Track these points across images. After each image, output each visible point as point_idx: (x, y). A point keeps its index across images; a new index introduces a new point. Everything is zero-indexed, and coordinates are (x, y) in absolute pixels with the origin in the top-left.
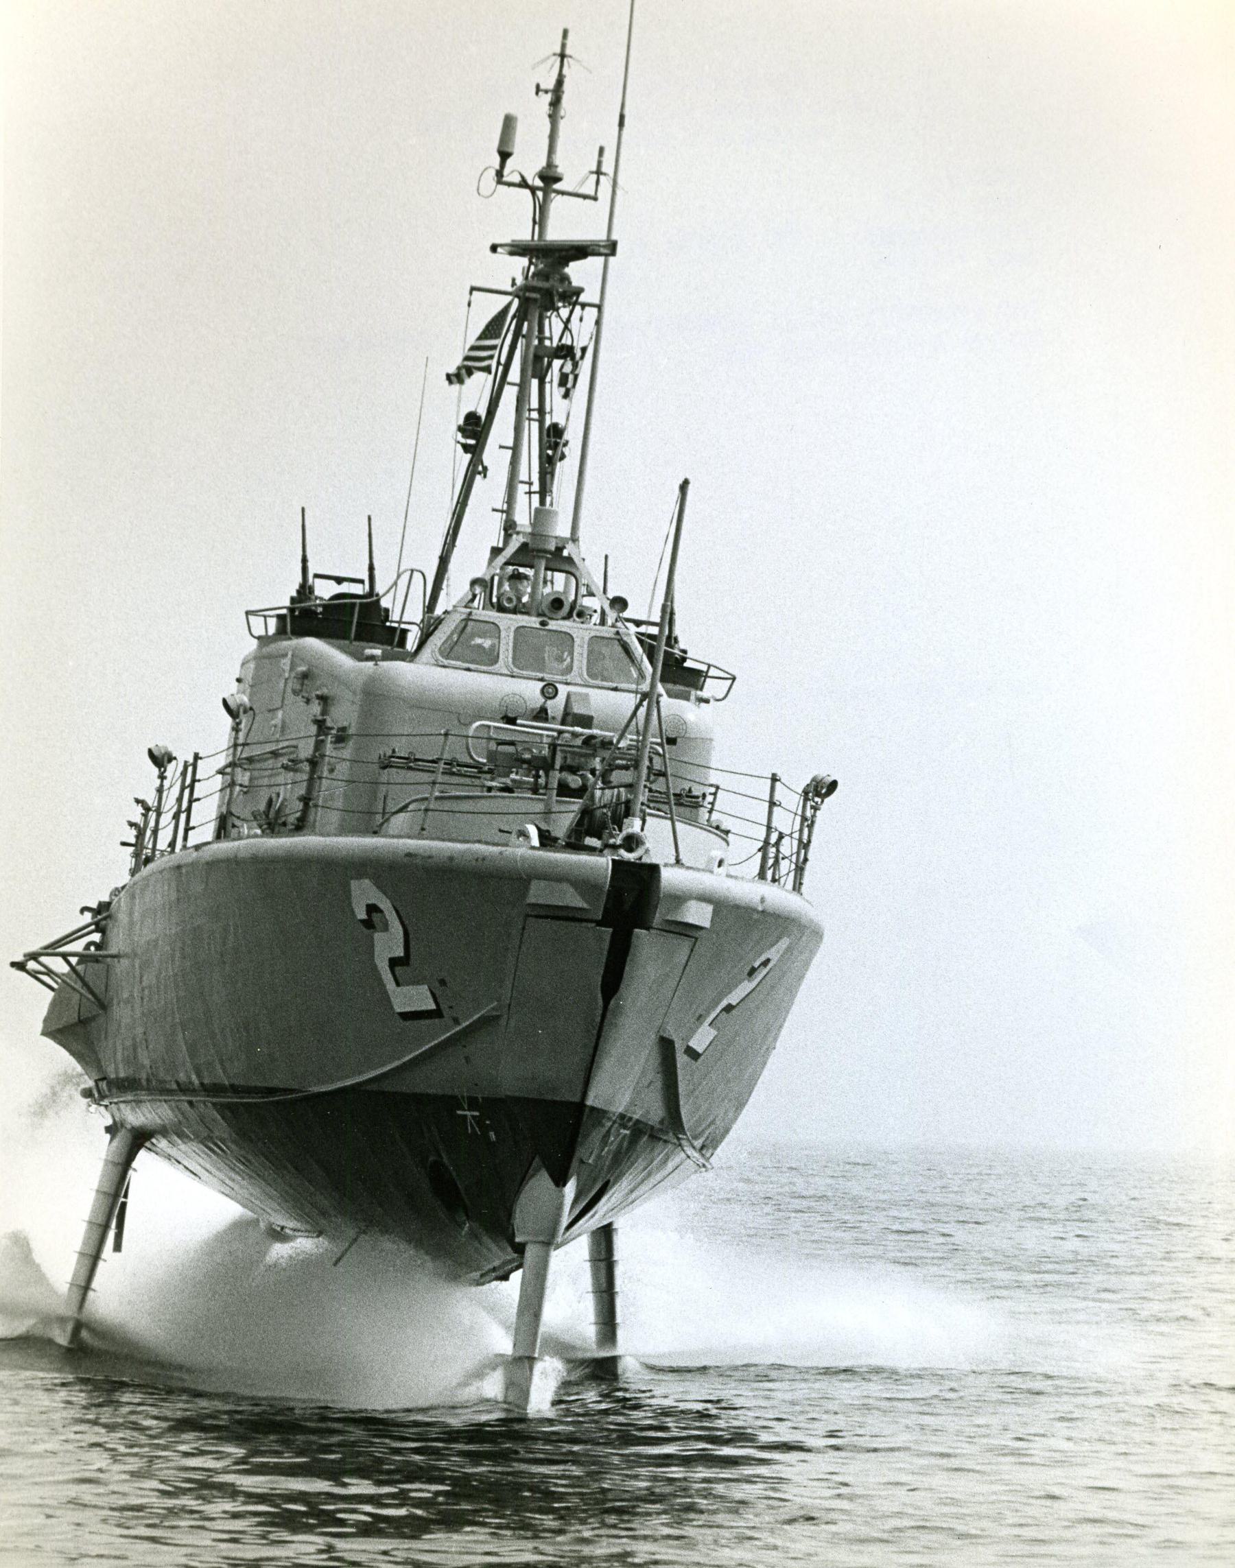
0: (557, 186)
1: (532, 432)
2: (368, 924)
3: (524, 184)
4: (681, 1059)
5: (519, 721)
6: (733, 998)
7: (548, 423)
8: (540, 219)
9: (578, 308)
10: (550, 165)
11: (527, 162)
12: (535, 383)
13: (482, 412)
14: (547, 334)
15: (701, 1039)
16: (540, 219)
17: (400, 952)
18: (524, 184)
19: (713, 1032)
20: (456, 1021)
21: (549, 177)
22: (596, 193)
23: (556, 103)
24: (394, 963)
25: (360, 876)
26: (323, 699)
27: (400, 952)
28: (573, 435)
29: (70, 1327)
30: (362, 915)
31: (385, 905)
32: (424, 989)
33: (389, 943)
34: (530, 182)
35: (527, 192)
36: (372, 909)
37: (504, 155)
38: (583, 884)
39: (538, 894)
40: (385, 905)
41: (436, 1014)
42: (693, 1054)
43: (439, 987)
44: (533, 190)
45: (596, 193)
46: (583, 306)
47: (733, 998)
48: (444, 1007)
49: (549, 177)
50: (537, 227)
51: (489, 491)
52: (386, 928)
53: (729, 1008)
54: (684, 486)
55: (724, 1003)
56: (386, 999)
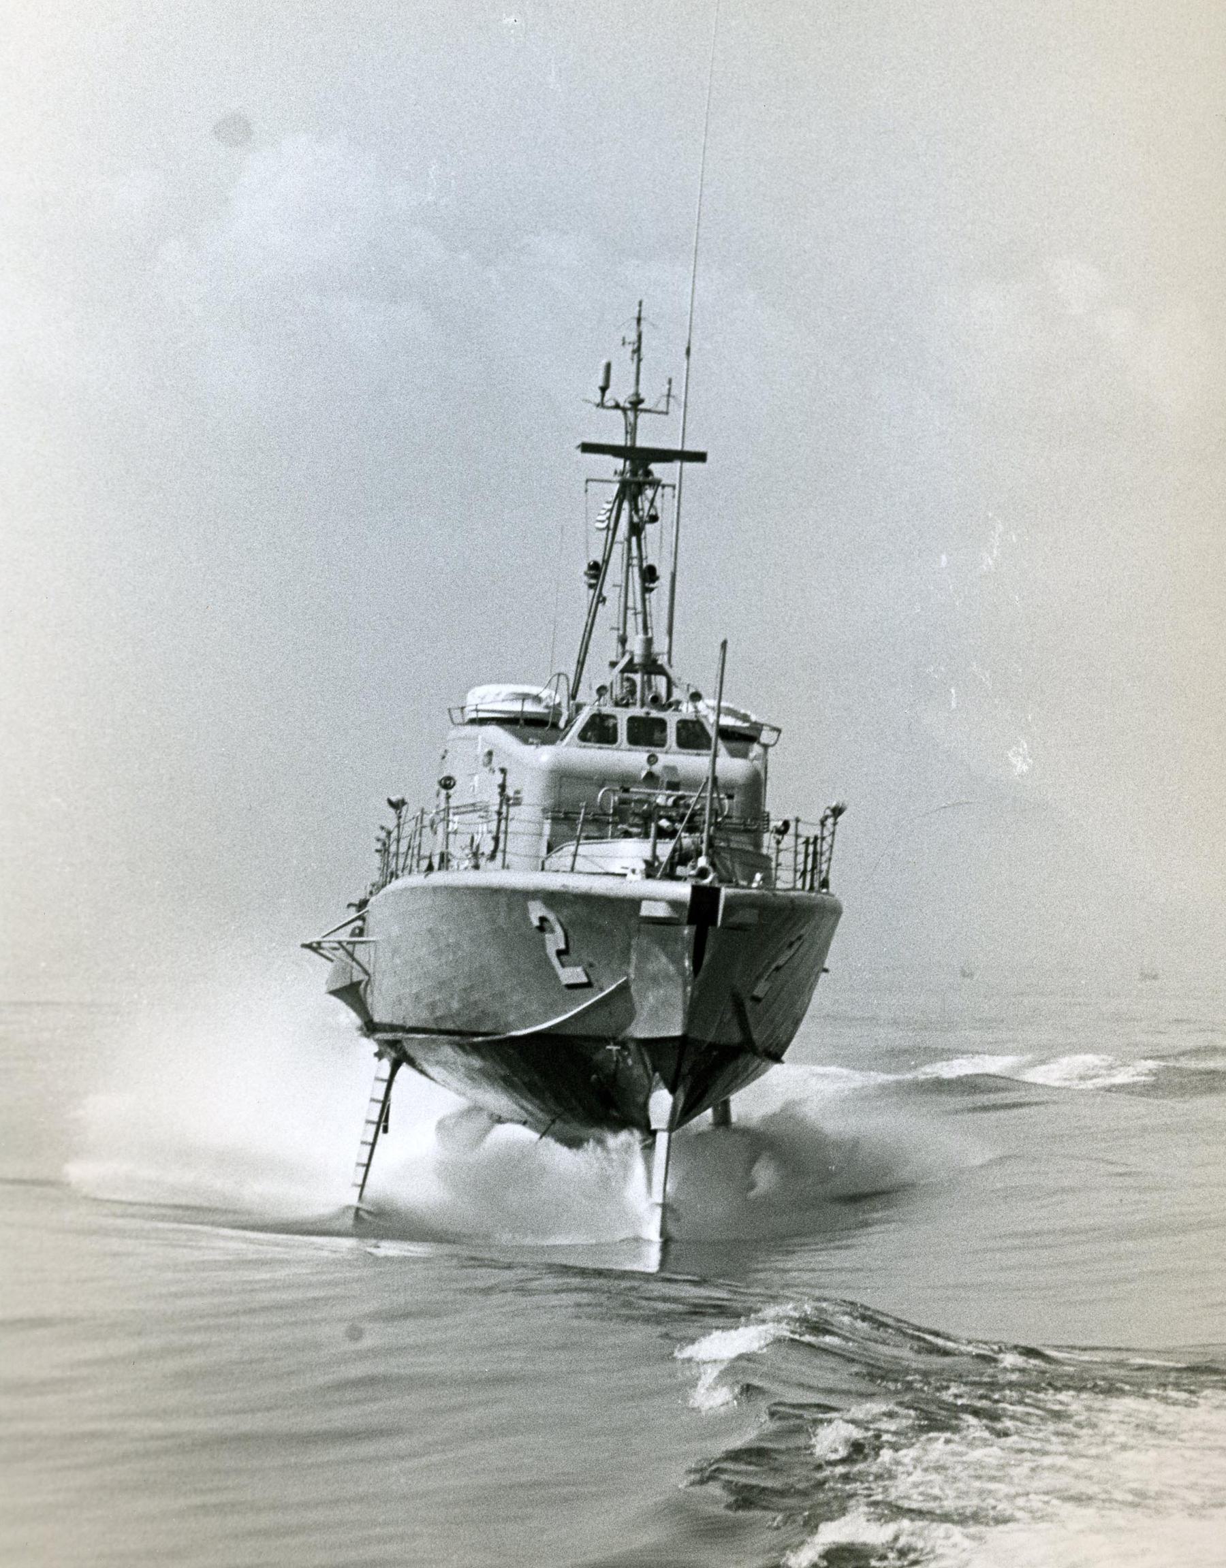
0: (641, 406)
1: (635, 573)
2: (541, 929)
3: (617, 406)
4: (749, 1004)
5: (632, 790)
6: (780, 962)
7: (645, 565)
8: (632, 430)
9: (660, 488)
10: (637, 394)
11: (621, 392)
12: (634, 539)
13: (600, 560)
14: (640, 507)
15: (760, 990)
16: (632, 430)
17: (562, 946)
18: (617, 406)
19: (768, 985)
20: (602, 990)
21: (636, 403)
22: (580, 873)
23: (638, 351)
24: (559, 953)
25: (534, 899)
26: (503, 771)
27: (562, 946)
28: (664, 573)
29: (354, 1211)
30: (536, 923)
31: (551, 917)
32: (579, 969)
33: (555, 941)
34: (622, 404)
35: (619, 412)
36: (543, 920)
37: (604, 389)
38: (674, 904)
39: (647, 910)
40: (551, 917)
41: (588, 985)
42: (757, 1000)
43: (589, 968)
44: (624, 410)
45: (580, 873)
46: (664, 486)
47: (780, 962)
48: (593, 980)
49: (636, 403)
50: (629, 437)
51: (609, 613)
52: (552, 931)
53: (778, 969)
54: (724, 645)
55: (773, 966)
56: (556, 977)
